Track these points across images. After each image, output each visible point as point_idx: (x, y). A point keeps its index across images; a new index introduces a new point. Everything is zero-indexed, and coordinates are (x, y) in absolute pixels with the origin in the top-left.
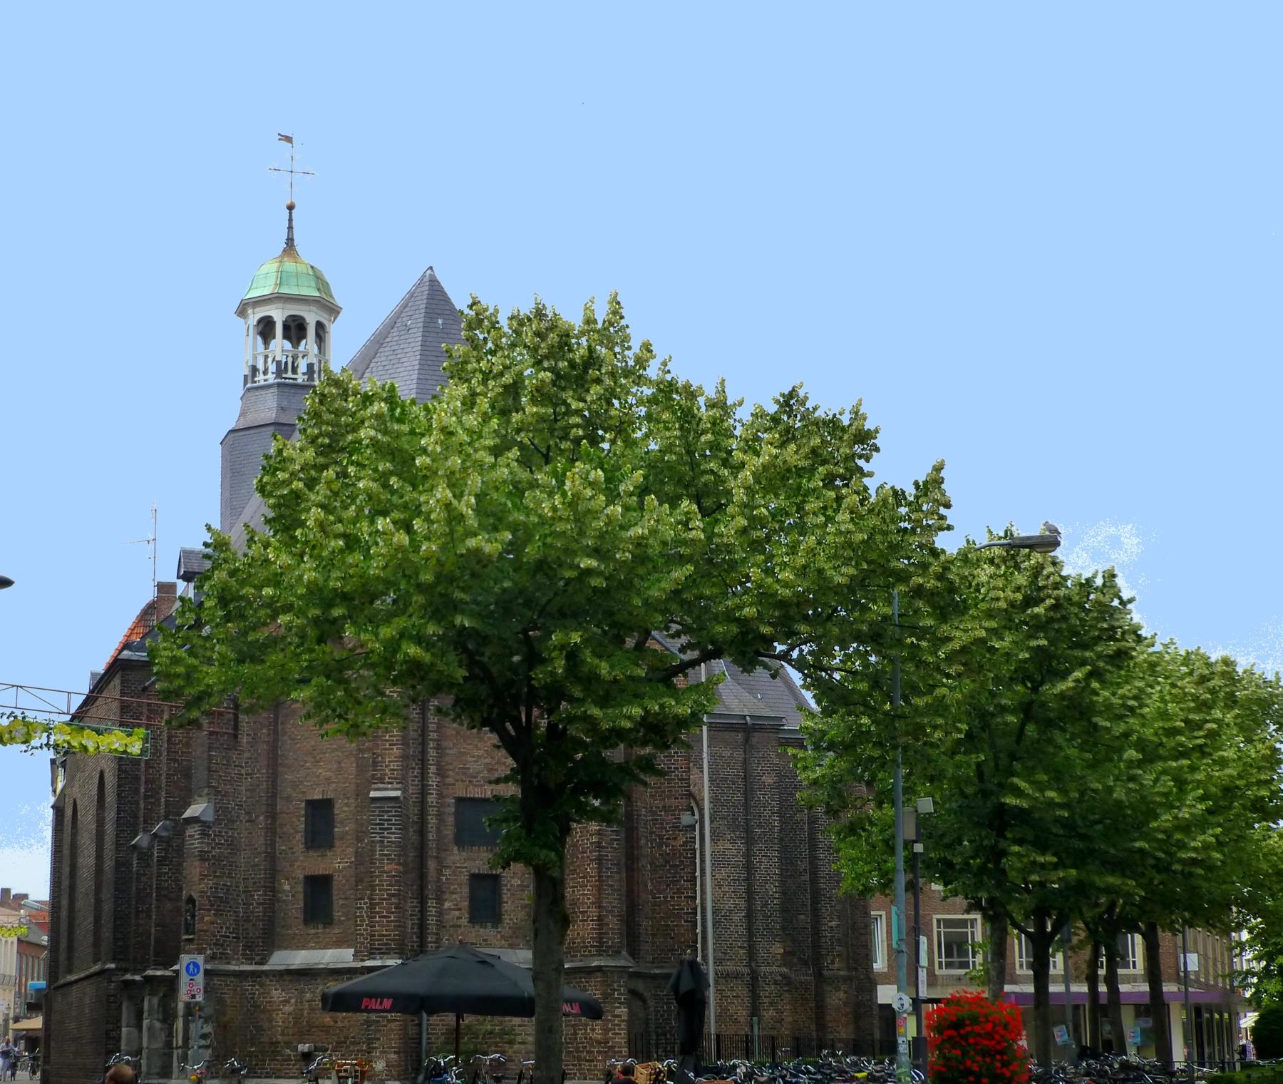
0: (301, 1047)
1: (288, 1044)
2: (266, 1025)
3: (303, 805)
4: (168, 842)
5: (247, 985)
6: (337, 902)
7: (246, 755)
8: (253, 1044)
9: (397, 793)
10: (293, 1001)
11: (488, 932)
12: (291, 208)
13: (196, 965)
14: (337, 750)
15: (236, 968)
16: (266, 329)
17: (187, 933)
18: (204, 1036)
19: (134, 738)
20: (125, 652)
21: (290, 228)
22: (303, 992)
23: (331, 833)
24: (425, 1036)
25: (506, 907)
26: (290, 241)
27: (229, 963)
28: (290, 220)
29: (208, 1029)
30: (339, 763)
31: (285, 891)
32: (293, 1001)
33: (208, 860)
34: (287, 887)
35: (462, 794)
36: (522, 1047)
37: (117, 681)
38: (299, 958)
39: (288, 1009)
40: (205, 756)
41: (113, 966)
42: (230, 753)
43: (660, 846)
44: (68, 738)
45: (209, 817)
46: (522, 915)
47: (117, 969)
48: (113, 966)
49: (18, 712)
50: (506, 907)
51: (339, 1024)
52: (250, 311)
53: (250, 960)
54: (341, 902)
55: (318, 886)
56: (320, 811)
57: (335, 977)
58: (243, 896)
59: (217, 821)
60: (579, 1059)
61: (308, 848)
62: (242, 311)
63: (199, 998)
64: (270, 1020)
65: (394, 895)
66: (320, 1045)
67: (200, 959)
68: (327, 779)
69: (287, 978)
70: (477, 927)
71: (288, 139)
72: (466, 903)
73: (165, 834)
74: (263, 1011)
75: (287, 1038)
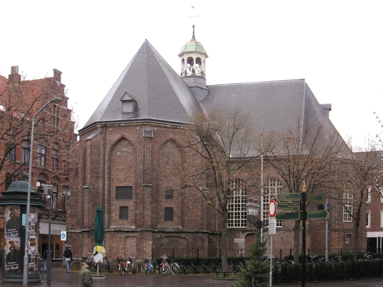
3: (115, 187)
11: (125, 222)
12: (194, 27)
21: (194, 32)
25: (129, 215)
26: (194, 36)
27: (76, 230)
28: (194, 30)
33: (69, 205)
35: (118, 186)
36: (131, 251)
43: (194, 197)
71: (193, 7)
72: (119, 214)
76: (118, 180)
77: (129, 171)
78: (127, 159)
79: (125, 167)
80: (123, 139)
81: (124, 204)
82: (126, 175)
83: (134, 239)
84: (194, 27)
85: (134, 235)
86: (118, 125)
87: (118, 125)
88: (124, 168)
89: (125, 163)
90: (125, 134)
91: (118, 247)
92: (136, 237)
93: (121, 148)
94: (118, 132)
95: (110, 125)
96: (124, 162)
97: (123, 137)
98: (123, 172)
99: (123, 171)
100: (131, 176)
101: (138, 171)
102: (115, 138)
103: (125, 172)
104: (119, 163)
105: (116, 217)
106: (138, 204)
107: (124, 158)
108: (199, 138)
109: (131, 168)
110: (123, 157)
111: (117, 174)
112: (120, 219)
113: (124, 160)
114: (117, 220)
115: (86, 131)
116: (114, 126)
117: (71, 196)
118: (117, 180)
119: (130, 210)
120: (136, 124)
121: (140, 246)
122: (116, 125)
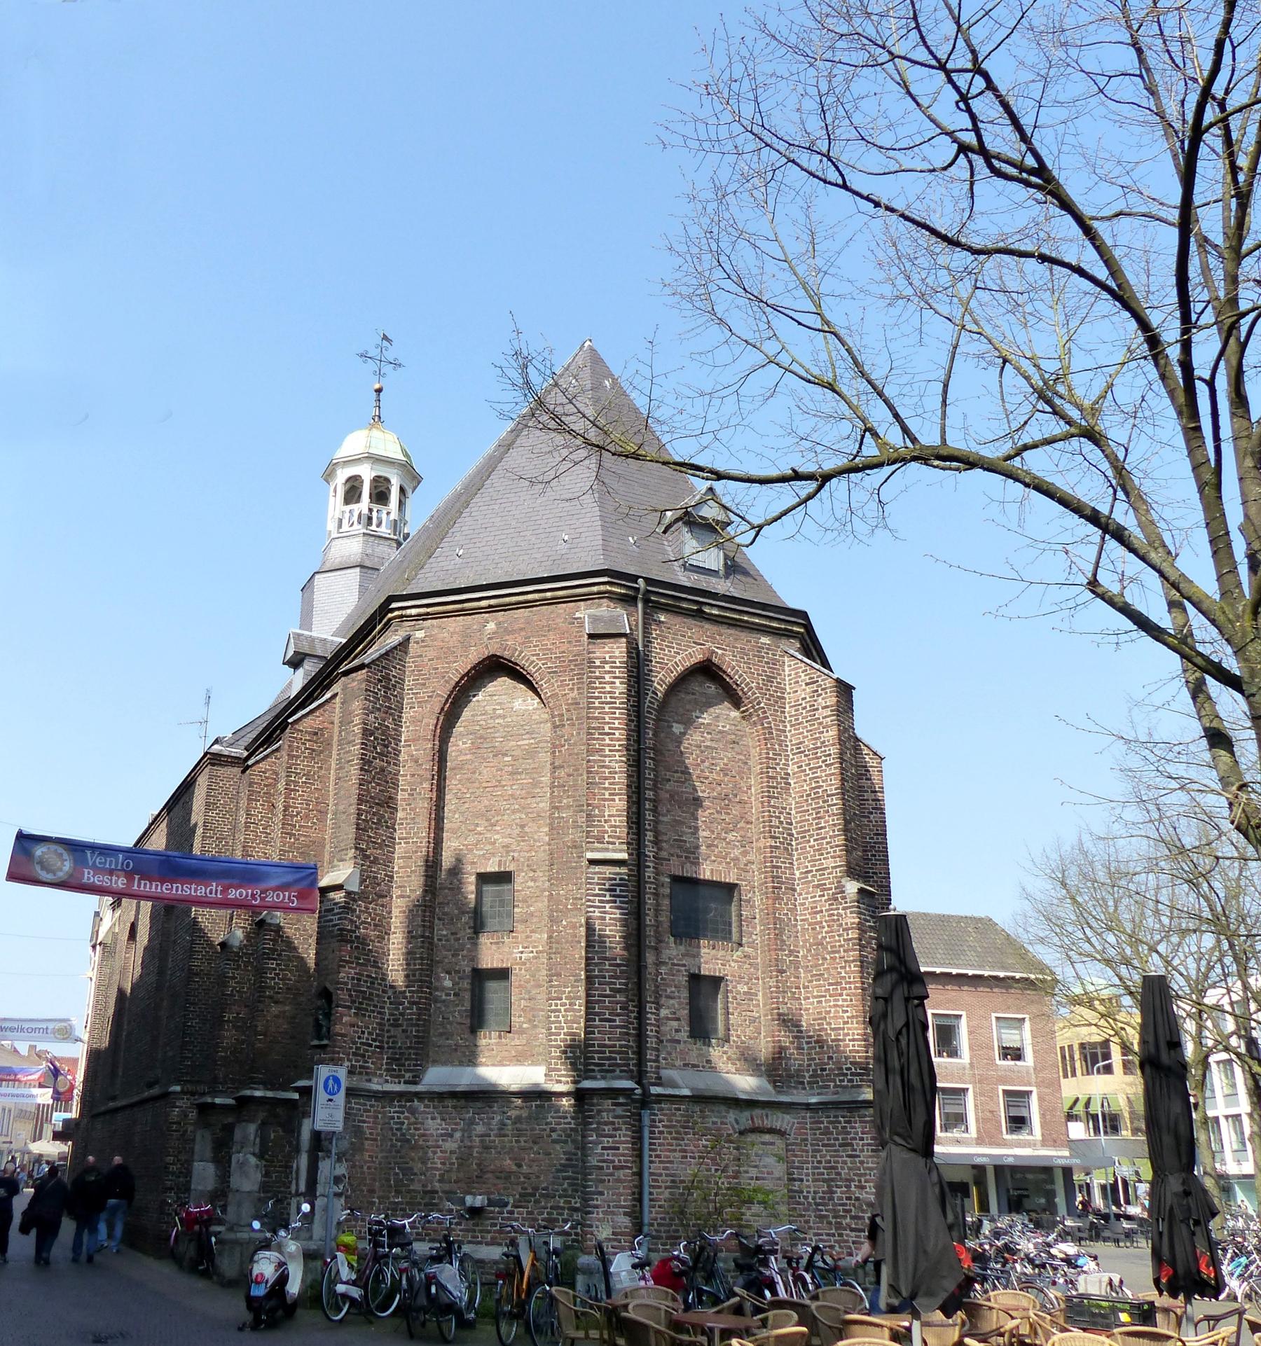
0: (469, 1200)
2: (418, 1167)
5: (391, 1111)
8: (398, 1192)
10: (458, 1135)
12: (379, 391)
13: (337, 1080)
14: (518, 811)
15: (379, 1088)
18: (337, 1180)
20: (216, 747)
22: (472, 1122)
23: (510, 915)
24: (646, 1190)
29: (341, 1170)
30: (522, 826)
31: (443, 989)
32: (458, 1135)
34: (448, 983)
39: (450, 1145)
40: (353, 809)
41: (178, 1088)
47: (182, 1092)
48: (178, 1088)
60: (839, 1226)
64: (424, 1161)
65: (619, 991)
66: (495, 1197)
67: (342, 1073)
69: (450, 1103)
70: (699, 1044)
72: (687, 1012)
74: (415, 1148)
75: (447, 1187)
76: (680, 847)
78: (713, 758)
80: (707, 670)
82: (713, 832)
83: (772, 1144)
85: (778, 1125)
90: (720, 652)
92: (781, 1133)
93: (688, 707)
96: (702, 771)
97: (709, 660)
100: (730, 837)
101: (775, 822)
102: (679, 657)
105: (675, 1024)
106: (785, 971)
108: (648, 761)
112: (691, 1036)
113: (703, 761)
114: (678, 1042)
115: (484, 603)
118: (672, 846)
121: (802, 1180)
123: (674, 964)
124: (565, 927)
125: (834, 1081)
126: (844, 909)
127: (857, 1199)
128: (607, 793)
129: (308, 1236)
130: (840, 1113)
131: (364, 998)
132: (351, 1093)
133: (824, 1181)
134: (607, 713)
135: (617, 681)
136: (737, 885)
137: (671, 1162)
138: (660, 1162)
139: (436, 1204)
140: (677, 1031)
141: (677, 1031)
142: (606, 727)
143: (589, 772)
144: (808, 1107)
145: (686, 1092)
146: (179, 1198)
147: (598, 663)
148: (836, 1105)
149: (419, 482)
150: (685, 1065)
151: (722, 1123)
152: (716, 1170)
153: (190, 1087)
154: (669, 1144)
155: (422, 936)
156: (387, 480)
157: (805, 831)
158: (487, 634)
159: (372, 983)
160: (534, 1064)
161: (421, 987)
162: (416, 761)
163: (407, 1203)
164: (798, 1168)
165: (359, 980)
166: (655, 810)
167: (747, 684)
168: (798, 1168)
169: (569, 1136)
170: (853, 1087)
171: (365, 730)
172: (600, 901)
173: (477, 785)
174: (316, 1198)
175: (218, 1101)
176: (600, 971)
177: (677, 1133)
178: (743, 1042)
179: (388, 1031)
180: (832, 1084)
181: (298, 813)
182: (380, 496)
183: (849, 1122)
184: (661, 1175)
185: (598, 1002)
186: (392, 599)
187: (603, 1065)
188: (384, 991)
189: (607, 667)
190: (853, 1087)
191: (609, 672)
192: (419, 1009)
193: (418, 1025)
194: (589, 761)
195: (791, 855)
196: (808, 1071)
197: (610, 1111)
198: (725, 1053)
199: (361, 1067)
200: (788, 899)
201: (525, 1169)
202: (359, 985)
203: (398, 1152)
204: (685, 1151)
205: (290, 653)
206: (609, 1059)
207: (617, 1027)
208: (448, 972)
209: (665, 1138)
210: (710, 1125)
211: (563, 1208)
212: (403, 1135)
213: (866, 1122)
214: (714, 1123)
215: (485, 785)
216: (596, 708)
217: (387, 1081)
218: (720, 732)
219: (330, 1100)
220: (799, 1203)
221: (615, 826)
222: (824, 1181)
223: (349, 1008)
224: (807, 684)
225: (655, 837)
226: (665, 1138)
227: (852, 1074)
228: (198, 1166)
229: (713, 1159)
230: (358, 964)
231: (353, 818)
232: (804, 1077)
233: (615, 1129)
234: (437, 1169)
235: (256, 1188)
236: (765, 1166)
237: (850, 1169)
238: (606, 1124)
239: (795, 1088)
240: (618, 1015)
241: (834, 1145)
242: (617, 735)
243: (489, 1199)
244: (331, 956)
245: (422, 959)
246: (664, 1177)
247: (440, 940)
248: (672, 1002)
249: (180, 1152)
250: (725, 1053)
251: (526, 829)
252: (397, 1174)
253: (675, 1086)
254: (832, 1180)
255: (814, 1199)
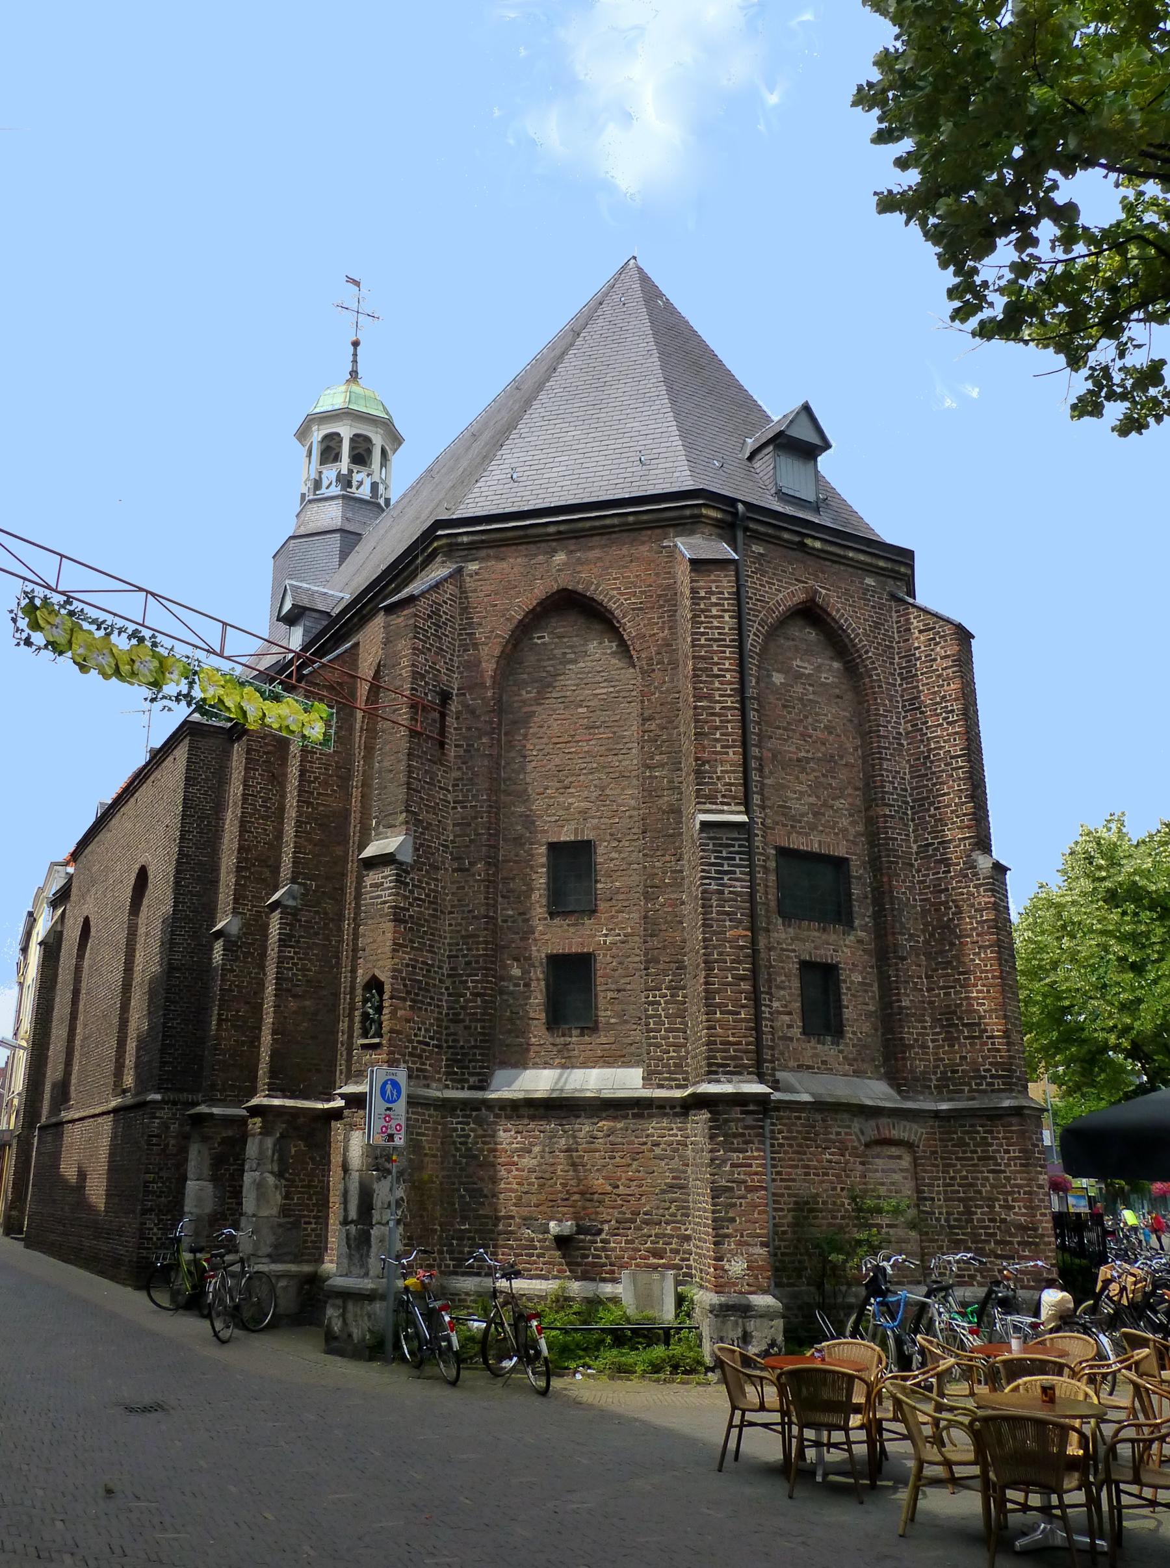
1: (527, 1221)
4: (294, 915)
5: (453, 1122)
6: (604, 995)
7: (456, 774)
8: (464, 1219)
9: (744, 818)
12: (356, 344)
13: (395, 1085)
15: (438, 1094)
16: (329, 451)
17: (365, 1035)
19: (315, 715)
21: (355, 361)
23: (591, 892)
31: (511, 978)
32: (536, 1149)
34: (516, 972)
37: (181, 753)
38: (538, 1081)
39: (527, 1161)
40: (402, 767)
41: (158, 1097)
42: (435, 767)
44: (221, 691)
45: (407, 857)
46: (866, 1027)
47: (163, 1101)
48: (158, 1097)
49: (146, 633)
50: (848, 1013)
51: (622, 1190)
52: (315, 428)
53: (460, 1083)
54: (610, 995)
55: (572, 975)
56: (573, 861)
57: (611, 1112)
58: (448, 983)
59: (417, 865)
61: (552, 915)
62: (302, 434)
63: (400, 1141)
67: (401, 1075)
68: (584, 812)
70: (813, 1042)
71: (357, 283)
72: (799, 1004)
73: (291, 903)
75: (525, 1211)
77: (831, 781)
78: (817, 714)
79: (808, 751)
81: (816, 948)
82: (818, 797)
83: (899, 1157)
84: (356, 344)
85: (905, 1136)
86: (797, 539)
87: (797, 539)
88: (808, 760)
89: (810, 737)
90: (824, 592)
91: (834, 1203)
92: (909, 1145)
93: (789, 654)
94: (792, 574)
95: (762, 529)
98: (802, 777)
99: (803, 770)
102: (781, 596)
103: (812, 777)
104: (785, 729)
105: (787, 1018)
107: (805, 706)
109: (835, 762)
110: (801, 700)
111: (778, 784)
112: (804, 1033)
113: (806, 717)
114: (791, 1039)
115: (552, 529)
116: (779, 538)
117: (412, 867)
119: (848, 989)
120: (868, 559)
121: (933, 1199)
122: (786, 536)
123: (783, 950)
124: (663, 905)
125: (969, 1085)
126: (976, 887)
127: (1003, 1221)
128: (718, 745)
129: (362, 1273)
130: (977, 1121)
131: (420, 989)
132: (413, 1102)
133: (960, 1200)
134: (716, 652)
135: (726, 615)
136: (847, 859)
137: (794, 1180)
138: (782, 1180)
139: (511, 1232)
140: (790, 1026)
141: (790, 1026)
142: (715, 669)
143: (697, 721)
144: (936, 1115)
145: (806, 1098)
146: (160, 1220)
147: (703, 594)
148: (972, 1113)
149: (400, 444)
150: (799, 1066)
151: (846, 1134)
152: (842, 1189)
153: (171, 1096)
154: (790, 1159)
155: (486, 917)
156: (368, 440)
157: (923, 799)
158: (557, 569)
159: (429, 971)
160: (627, 1065)
161: (486, 975)
162: (473, 712)
163: (476, 1231)
164: (929, 1185)
165: (414, 967)
166: (760, 770)
167: (854, 630)
168: (929, 1185)
169: (676, 1150)
170: (992, 1091)
171: (414, 672)
172: (717, 872)
173: (544, 740)
174: (371, 1226)
175: (215, 1111)
176: (720, 954)
177: (800, 1145)
178: (859, 1039)
179: (447, 1028)
180: (967, 1088)
181: (316, 778)
182: (360, 457)
183: (991, 1132)
184: (782, 1195)
185: (718, 991)
186: (439, 524)
187: (728, 1065)
188: (441, 981)
189: (714, 600)
190: (992, 1091)
191: (716, 604)
192: (484, 1001)
193: (484, 1021)
194: (696, 708)
195: (906, 825)
196: (935, 1073)
197: (739, 1120)
198: (841, 1052)
199: (418, 1070)
200: (906, 876)
201: (622, 1190)
202: (414, 973)
203: (462, 1169)
204: (807, 1167)
205: (288, 606)
206: (733, 1058)
207: (742, 1020)
208: (517, 959)
209: (786, 1152)
210: (833, 1137)
211: (672, 1236)
212: (470, 1149)
213: (1011, 1132)
214: (838, 1134)
215: (557, 740)
216: (702, 646)
217: (447, 1087)
218: (823, 684)
219: (389, 1109)
220: (931, 1226)
221: (731, 784)
222: (960, 1200)
223: (404, 999)
224: (920, 632)
225: (763, 800)
226: (786, 1152)
227: (992, 1077)
228: (191, 1186)
229: (838, 1176)
230: (412, 948)
231: (403, 778)
232: (931, 1080)
233: (746, 1142)
234: (512, 1190)
235: (275, 1211)
236: (893, 1184)
237: (992, 1186)
238: (735, 1136)
239: (922, 1093)
240: (743, 1006)
241: (973, 1159)
242: (728, 676)
243: (578, 1225)
244: (380, 939)
245: (486, 942)
246: (786, 1198)
247: (505, 921)
248: (782, 993)
249: (161, 1169)
250: (841, 1052)
251: (608, 792)
252: (463, 1197)
253: (790, 1089)
254: (971, 1199)
255: (947, 1220)
